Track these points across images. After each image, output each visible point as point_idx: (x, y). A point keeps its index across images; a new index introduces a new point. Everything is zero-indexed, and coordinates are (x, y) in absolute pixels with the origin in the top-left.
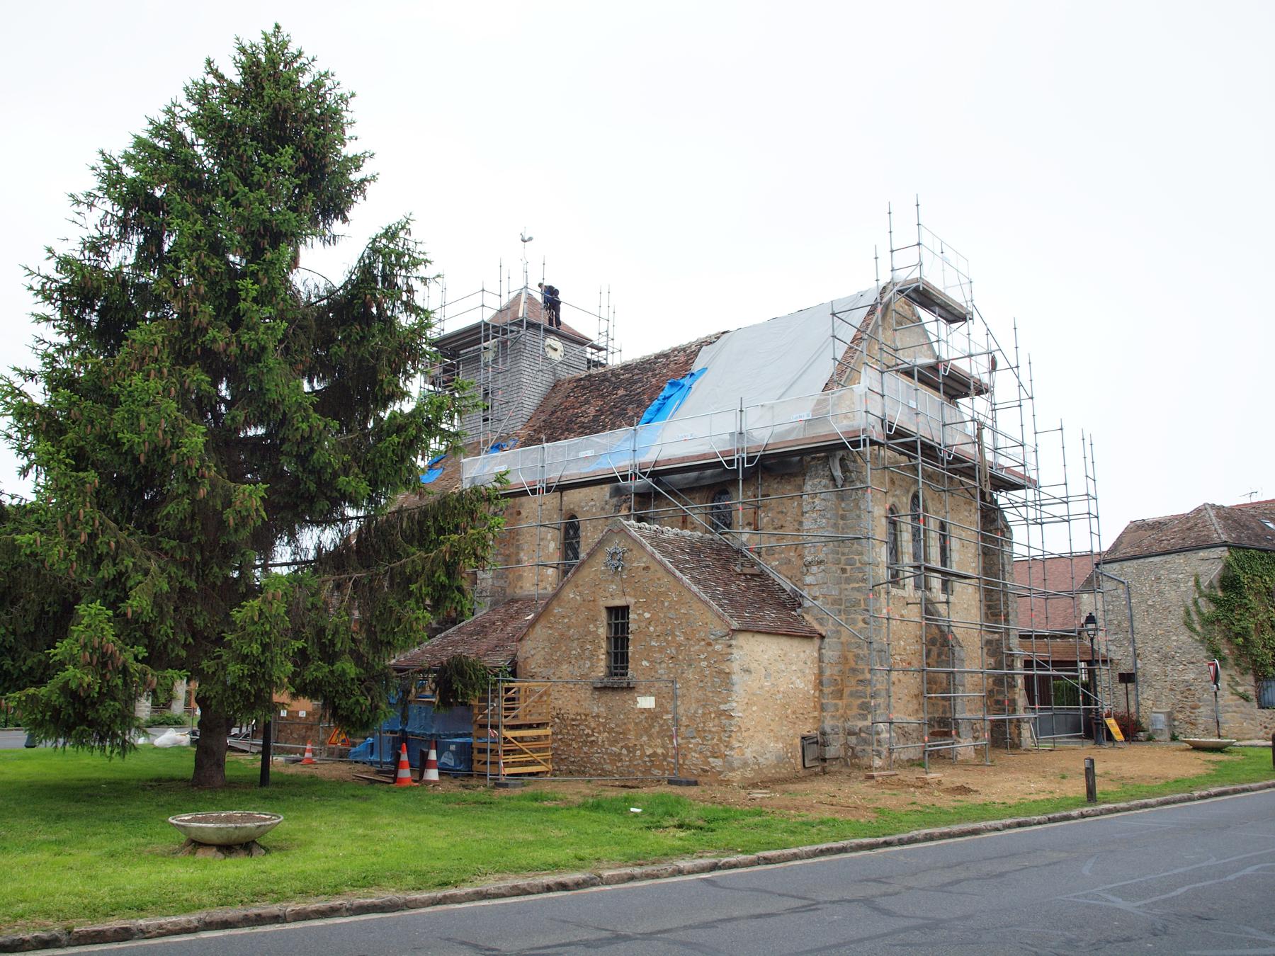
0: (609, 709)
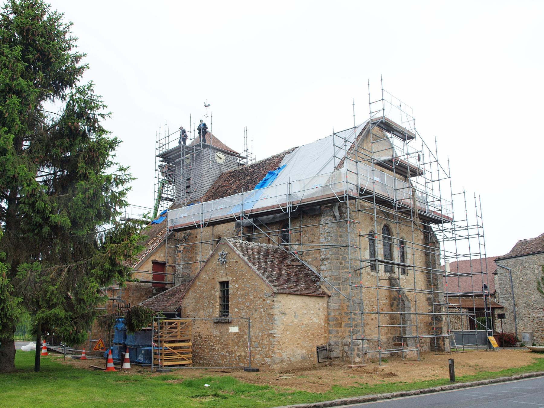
0: (221, 333)
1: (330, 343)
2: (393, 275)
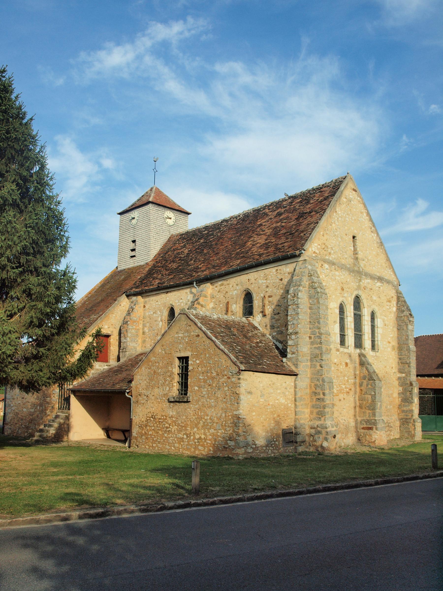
1: (296, 425)
2: (363, 351)
